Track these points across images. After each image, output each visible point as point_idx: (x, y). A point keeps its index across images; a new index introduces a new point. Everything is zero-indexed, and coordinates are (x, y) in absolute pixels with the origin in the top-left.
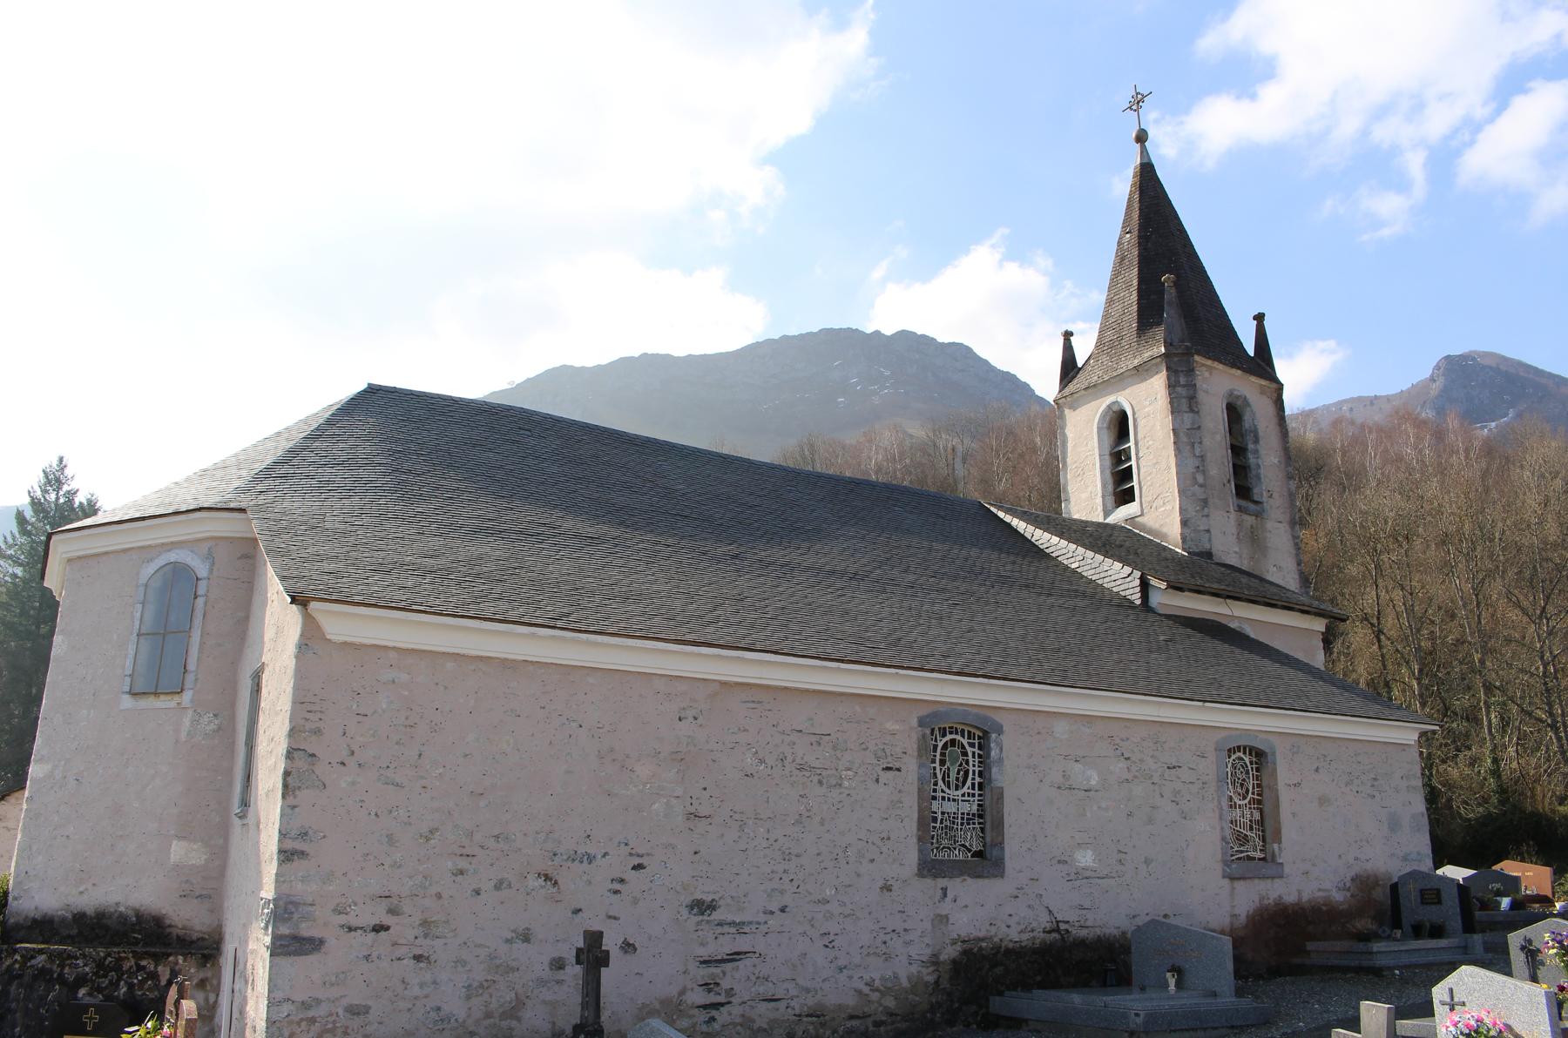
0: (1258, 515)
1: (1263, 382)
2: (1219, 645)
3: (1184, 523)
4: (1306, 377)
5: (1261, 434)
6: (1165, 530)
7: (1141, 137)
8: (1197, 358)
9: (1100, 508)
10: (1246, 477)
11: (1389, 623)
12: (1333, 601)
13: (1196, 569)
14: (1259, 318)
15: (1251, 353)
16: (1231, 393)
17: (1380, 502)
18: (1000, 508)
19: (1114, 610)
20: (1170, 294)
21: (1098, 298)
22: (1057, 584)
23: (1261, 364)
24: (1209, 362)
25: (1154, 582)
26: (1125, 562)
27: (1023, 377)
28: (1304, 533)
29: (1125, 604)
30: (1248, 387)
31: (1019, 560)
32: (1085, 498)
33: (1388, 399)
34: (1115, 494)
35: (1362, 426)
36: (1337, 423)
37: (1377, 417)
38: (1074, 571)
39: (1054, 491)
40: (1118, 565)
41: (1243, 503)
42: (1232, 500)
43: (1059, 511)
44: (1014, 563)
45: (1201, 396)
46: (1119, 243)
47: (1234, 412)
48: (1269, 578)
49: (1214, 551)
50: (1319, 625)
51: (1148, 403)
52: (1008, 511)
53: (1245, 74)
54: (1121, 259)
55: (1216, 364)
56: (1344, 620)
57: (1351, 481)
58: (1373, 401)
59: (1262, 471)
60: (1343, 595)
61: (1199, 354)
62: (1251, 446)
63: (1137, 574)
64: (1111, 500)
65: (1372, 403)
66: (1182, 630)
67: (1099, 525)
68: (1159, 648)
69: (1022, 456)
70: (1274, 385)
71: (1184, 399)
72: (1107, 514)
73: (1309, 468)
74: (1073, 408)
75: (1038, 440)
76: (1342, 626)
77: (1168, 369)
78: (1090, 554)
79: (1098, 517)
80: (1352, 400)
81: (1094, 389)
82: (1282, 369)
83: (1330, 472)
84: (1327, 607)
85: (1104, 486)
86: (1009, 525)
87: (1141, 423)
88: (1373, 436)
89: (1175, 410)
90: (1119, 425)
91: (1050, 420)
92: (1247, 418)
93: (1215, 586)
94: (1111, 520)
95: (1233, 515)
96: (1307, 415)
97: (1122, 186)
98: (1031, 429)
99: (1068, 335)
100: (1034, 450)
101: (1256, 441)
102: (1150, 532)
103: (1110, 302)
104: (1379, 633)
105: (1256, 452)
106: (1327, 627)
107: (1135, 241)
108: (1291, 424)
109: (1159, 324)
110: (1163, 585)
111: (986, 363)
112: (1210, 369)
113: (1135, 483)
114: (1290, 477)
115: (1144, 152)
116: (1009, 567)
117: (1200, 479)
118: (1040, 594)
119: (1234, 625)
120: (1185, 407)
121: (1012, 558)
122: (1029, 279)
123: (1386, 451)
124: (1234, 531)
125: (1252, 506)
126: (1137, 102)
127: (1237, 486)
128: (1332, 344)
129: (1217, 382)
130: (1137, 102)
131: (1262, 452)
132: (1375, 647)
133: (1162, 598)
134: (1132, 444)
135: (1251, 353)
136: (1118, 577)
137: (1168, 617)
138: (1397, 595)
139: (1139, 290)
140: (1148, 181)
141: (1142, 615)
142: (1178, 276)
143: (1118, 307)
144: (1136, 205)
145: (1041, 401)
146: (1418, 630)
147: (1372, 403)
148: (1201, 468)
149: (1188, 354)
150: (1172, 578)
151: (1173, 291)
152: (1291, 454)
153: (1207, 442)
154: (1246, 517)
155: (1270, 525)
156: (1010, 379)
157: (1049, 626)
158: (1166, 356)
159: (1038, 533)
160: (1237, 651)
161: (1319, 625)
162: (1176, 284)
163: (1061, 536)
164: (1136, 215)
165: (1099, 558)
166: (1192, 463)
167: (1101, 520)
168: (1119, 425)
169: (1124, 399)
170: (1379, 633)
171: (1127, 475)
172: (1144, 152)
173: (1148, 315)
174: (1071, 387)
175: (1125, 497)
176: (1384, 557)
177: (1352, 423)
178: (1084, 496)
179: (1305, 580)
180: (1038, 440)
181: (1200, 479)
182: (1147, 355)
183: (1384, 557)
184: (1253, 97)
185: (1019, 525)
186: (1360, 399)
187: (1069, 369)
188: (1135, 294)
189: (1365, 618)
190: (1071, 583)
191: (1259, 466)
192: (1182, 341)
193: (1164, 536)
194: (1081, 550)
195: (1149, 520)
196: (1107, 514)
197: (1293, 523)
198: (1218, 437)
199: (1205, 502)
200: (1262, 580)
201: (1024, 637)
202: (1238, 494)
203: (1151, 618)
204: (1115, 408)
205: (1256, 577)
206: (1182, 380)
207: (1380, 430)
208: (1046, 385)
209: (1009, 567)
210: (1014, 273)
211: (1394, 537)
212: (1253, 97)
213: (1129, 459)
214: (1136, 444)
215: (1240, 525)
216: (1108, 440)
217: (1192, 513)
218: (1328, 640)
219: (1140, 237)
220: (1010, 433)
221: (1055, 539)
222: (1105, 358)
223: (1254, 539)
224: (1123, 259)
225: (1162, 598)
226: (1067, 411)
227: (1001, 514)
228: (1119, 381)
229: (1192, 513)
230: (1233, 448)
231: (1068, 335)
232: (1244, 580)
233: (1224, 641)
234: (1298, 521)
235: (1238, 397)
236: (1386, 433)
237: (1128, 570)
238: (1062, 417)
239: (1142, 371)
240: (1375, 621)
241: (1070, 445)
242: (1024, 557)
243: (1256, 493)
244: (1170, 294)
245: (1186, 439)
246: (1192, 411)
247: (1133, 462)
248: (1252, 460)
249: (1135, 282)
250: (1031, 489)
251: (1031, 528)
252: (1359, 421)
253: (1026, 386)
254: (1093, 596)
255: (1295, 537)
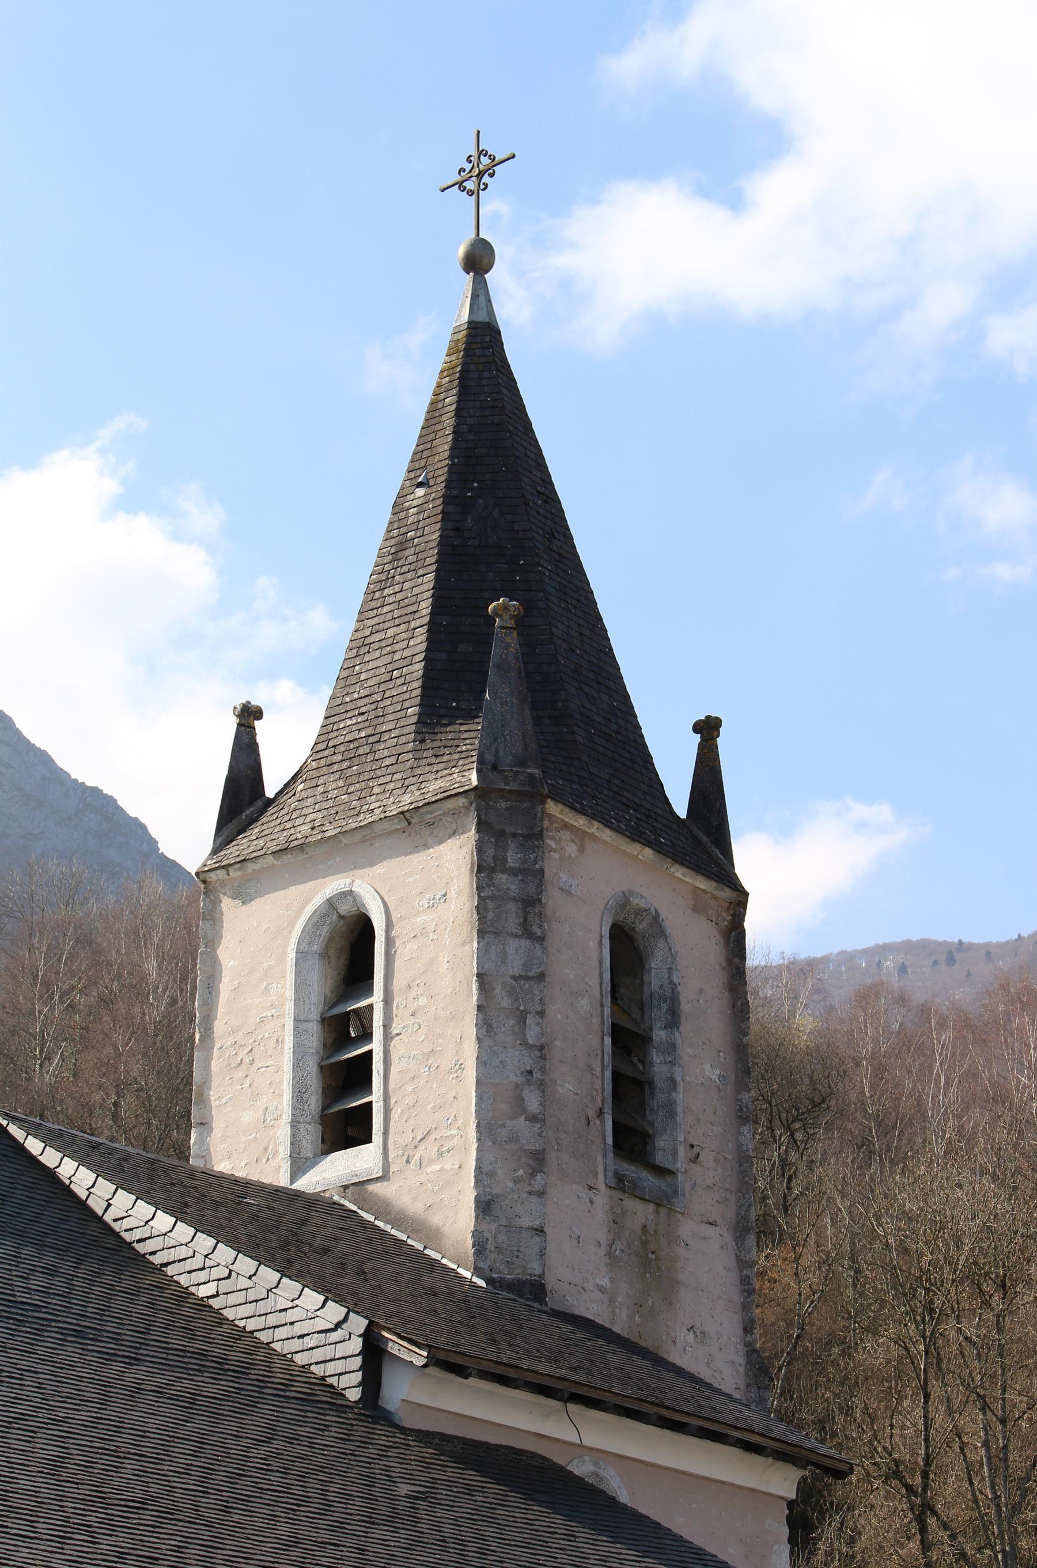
0: (662, 1201)
1: (702, 883)
2: (541, 1517)
3: (484, 1207)
4: (808, 887)
5: (685, 1007)
6: (436, 1219)
7: (478, 260)
8: (553, 808)
9: (284, 1151)
10: (642, 1106)
11: (950, 1491)
12: (822, 1423)
13: (506, 1321)
14: (708, 729)
15: (681, 807)
16: (624, 903)
17: (953, 1197)
18: (32, 1129)
19: (291, 1411)
20: (505, 644)
21: (329, 626)
22: (156, 1334)
23: (701, 839)
24: (581, 822)
25: (396, 1346)
26: (331, 1292)
27: (132, 806)
28: (768, 1258)
29: (320, 1395)
30: (664, 890)
31: (66, 1267)
32: (249, 1118)
33: (988, 952)
34: (325, 1120)
35: (925, 1012)
36: (866, 997)
37: (960, 993)
38: (203, 1305)
39: (174, 1098)
40: (312, 1299)
41: (629, 1169)
42: (602, 1161)
43: (182, 1152)
44: (52, 1272)
45: (553, 900)
46: (398, 507)
47: (629, 947)
48: (675, 1357)
49: (550, 1282)
50: (783, 1482)
51: (427, 902)
52: (50, 1139)
53: (718, 144)
54: (397, 546)
55: (595, 828)
56: (841, 1475)
57: (886, 1140)
58: (954, 953)
59: (680, 1096)
60: (848, 1411)
61: (558, 798)
62: (659, 1034)
63: (358, 1324)
64: (312, 1133)
65: (951, 960)
66: (453, 1472)
67: (277, 1192)
68: (394, 1514)
69: (106, 1001)
70: (727, 894)
71: (511, 904)
72: (299, 1166)
73: (798, 1097)
74: (243, 896)
75: (152, 967)
76: (839, 1489)
77: (482, 826)
78: (246, 1264)
79: (276, 1174)
80: (908, 947)
81: (299, 856)
82: (751, 858)
83: (841, 1113)
84: (809, 1440)
85: (299, 1095)
86: (50, 1175)
87: (404, 951)
88: (947, 1035)
89: (487, 927)
90: (351, 951)
91: (184, 920)
92: (656, 963)
93: (545, 1368)
94: (309, 1183)
95: (603, 1198)
96: (802, 971)
97: (406, 383)
98: (137, 936)
99: (249, 715)
100: (139, 991)
101: (674, 1021)
102: (400, 1220)
103: (359, 647)
104: (923, 1511)
105: (671, 1048)
106: (803, 1486)
107: (435, 506)
108: (761, 992)
109: (470, 715)
110: (418, 1357)
111: (44, 759)
112: (581, 837)
113: (376, 1097)
114: (744, 1117)
115: (480, 295)
116: (38, 1281)
117: (533, 1102)
118: (109, 1357)
119: (580, 1468)
120: (512, 924)
121: (49, 1259)
122: (173, 561)
123: (972, 1074)
124: (602, 1235)
125: (648, 1179)
126: (479, 172)
127: (618, 1128)
128: (884, 812)
129: (595, 871)
130: (479, 172)
131: (685, 1050)
132: (914, 1545)
133: (416, 1391)
134: (376, 999)
135: (681, 807)
136: (308, 1326)
137: (425, 1437)
138: (972, 1421)
139: (434, 627)
140: (481, 366)
141: (360, 1430)
142: (528, 606)
143: (377, 661)
144: (448, 421)
145: (170, 868)
146: (1015, 1509)
147: (951, 960)
148: (537, 1077)
149: (533, 795)
150: (442, 1341)
151: (513, 638)
152: (748, 1057)
153: (556, 1011)
154: (630, 1203)
155: (687, 1228)
156: (99, 807)
157: (124, 1442)
158: (479, 793)
159: (123, 1199)
160: (583, 1533)
161: (783, 1482)
162: (521, 623)
163: (180, 1213)
164: (444, 446)
165: (269, 1275)
166: (517, 1060)
167: (282, 1179)
168: (351, 951)
169: (371, 887)
170: (923, 1511)
171: (354, 1075)
172: (480, 295)
173: (448, 690)
174: (243, 845)
175: (347, 1128)
176: (949, 1327)
177: (902, 1000)
178: (247, 1117)
179: (758, 1369)
180: (152, 967)
181: (533, 1102)
182: (434, 787)
183: (949, 1327)
184: (735, 202)
185: (79, 1177)
186: (923, 947)
187: (244, 797)
188: (420, 641)
189: (895, 1472)
190: (190, 1333)
191: (673, 1083)
192: (522, 763)
193: (432, 1236)
194: (225, 1253)
195: (402, 1192)
196: (299, 1166)
197: (741, 1229)
198: (584, 1004)
199: (538, 1161)
200: (659, 1362)
201: (55, 1466)
202: (617, 1146)
203: (382, 1436)
204: (345, 908)
205: (644, 1353)
206: (513, 857)
207: (964, 1023)
208: (184, 828)
209: (38, 1281)
210: (141, 538)
211: (973, 1277)
212: (735, 202)
213: (366, 1036)
214: (387, 1001)
215: (617, 1221)
216: (321, 983)
217: (504, 1183)
218: (803, 1522)
219: (448, 499)
220: (84, 941)
221: (164, 1221)
222: (332, 784)
223: (648, 1261)
224: (402, 546)
225: (416, 1391)
226: (227, 904)
227: (34, 1145)
228: (361, 842)
229: (504, 1183)
230: (618, 1033)
231: (249, 715)
232: (616, 1358)
233: (554, 1507)
234: (758, 1226)
235: (640, 912)
236: (977, 1032)
237: (335, 1311)
238: (213, 915)
239: (417, 825)
240: (918, 1481)
241: (225, 987)
242: (80, 1260)
243: (664, 1147)
244: (505, 644)
245: (509, 1000)
246: (527, 933)
247: (376, 1046)
248: (658, 1067)
249: (425, 607)
250: (121, 1088)
251: (105, 1187)
252: (918, 998)
253: (138, 828)
254: (243, 1370)
255: (743, 1264)
